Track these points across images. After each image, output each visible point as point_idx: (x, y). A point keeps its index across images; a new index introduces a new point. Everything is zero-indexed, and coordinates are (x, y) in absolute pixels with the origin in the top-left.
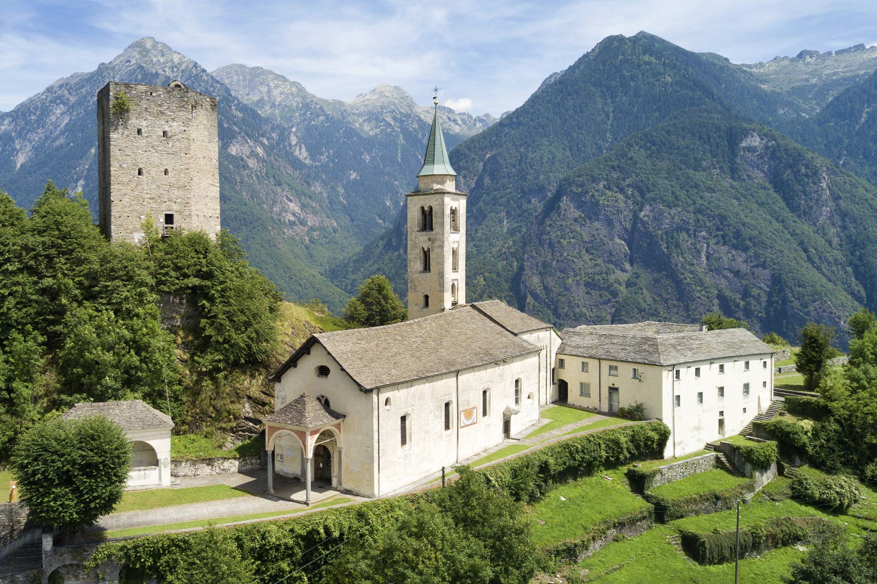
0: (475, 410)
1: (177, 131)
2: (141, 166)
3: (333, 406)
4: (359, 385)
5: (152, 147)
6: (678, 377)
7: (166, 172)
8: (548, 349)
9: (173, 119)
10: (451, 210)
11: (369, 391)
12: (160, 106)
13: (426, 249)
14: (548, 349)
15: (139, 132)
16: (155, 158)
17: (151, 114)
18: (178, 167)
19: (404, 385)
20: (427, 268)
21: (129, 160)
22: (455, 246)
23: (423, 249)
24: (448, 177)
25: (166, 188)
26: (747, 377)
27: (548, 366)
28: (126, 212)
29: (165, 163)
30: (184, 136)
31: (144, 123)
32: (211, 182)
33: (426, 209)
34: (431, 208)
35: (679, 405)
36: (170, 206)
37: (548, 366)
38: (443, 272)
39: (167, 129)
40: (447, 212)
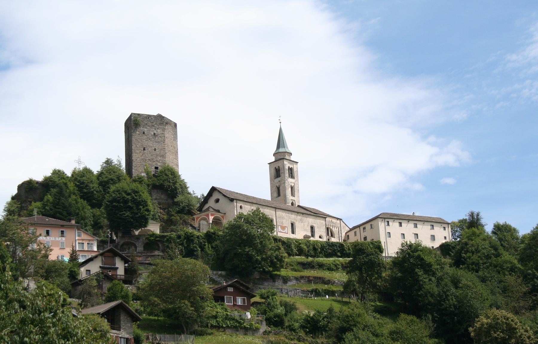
0: (286, 228)
1: (160, 133)
2: (145, 146)
3: (221, 211)
4: (229, 198)
5: (149, 139)
6: (388, 225)
7: (155, 150)
8: (340, 229)
9: (158, 129)
10: (289, 167)
11: (232, 200)
12: (152, 123)
13: (278, 186)
14: (340, 229)
15: (144, 133)
16: (150, 143)
17: (149, 126)
18: (160, 148)
19: (249, 204)
20: (279, 195)
21: (140, 144)
22: (293, 185)
23: (277, 186)
24: (286, 154)
25: (155, 156)
26: (432, 232)
27: (340, 238)
28: (138, 165)
29: (155, 146)
30: (163, 135)
31: (146, 130)
32: (174, 157)
33: (277, 168)
34: (279, 167)
35: (390, 237)
36: (157, 163)
37: (340, 238)
38: (286, 195)
39: (155, 132)
40: (287, 168)
